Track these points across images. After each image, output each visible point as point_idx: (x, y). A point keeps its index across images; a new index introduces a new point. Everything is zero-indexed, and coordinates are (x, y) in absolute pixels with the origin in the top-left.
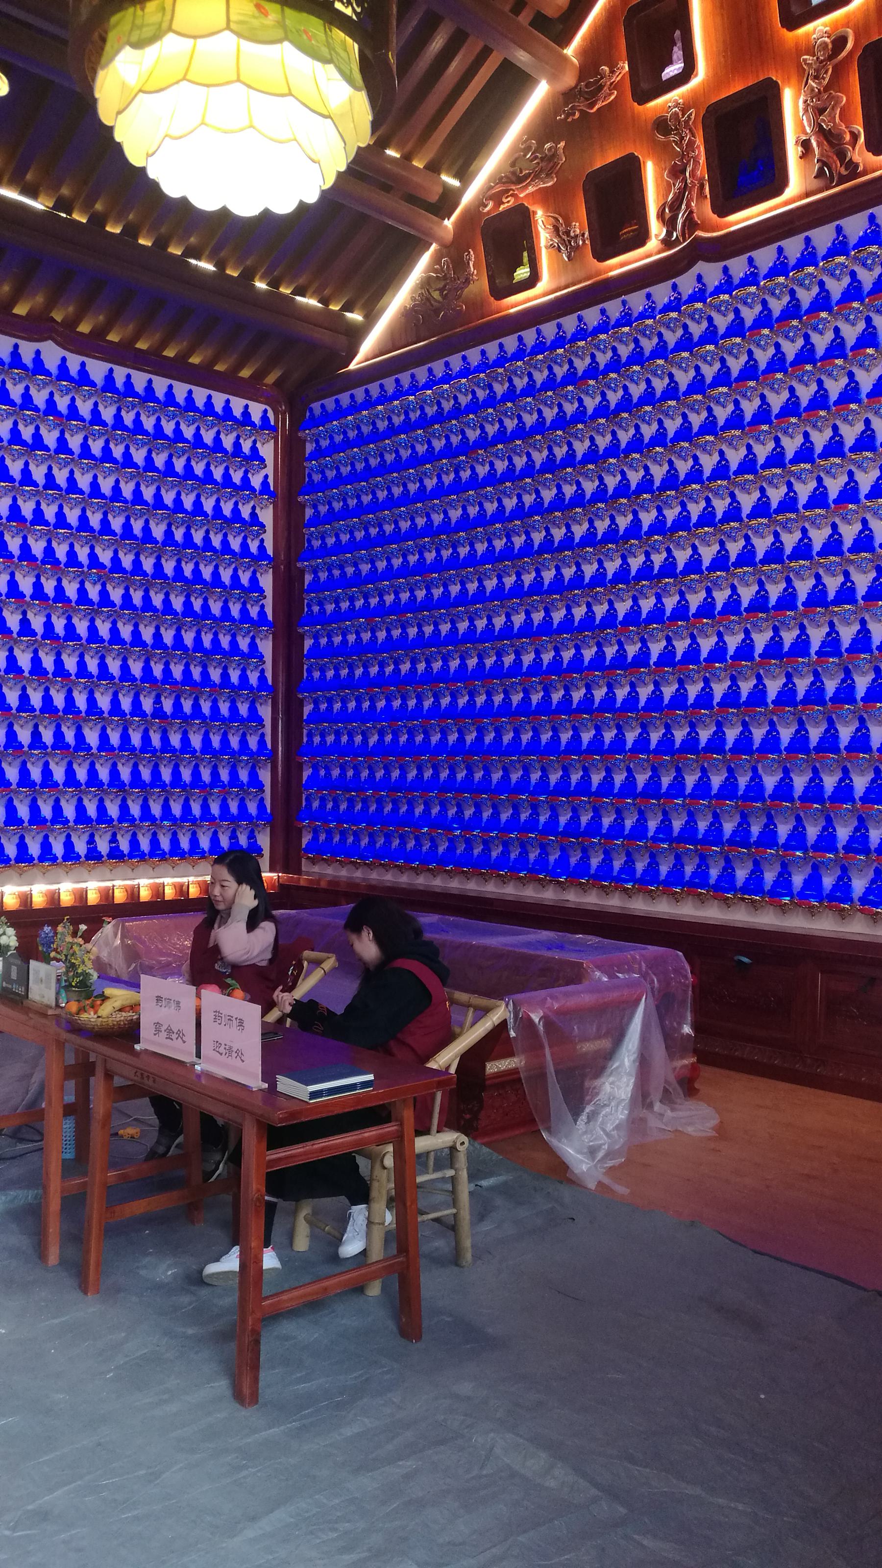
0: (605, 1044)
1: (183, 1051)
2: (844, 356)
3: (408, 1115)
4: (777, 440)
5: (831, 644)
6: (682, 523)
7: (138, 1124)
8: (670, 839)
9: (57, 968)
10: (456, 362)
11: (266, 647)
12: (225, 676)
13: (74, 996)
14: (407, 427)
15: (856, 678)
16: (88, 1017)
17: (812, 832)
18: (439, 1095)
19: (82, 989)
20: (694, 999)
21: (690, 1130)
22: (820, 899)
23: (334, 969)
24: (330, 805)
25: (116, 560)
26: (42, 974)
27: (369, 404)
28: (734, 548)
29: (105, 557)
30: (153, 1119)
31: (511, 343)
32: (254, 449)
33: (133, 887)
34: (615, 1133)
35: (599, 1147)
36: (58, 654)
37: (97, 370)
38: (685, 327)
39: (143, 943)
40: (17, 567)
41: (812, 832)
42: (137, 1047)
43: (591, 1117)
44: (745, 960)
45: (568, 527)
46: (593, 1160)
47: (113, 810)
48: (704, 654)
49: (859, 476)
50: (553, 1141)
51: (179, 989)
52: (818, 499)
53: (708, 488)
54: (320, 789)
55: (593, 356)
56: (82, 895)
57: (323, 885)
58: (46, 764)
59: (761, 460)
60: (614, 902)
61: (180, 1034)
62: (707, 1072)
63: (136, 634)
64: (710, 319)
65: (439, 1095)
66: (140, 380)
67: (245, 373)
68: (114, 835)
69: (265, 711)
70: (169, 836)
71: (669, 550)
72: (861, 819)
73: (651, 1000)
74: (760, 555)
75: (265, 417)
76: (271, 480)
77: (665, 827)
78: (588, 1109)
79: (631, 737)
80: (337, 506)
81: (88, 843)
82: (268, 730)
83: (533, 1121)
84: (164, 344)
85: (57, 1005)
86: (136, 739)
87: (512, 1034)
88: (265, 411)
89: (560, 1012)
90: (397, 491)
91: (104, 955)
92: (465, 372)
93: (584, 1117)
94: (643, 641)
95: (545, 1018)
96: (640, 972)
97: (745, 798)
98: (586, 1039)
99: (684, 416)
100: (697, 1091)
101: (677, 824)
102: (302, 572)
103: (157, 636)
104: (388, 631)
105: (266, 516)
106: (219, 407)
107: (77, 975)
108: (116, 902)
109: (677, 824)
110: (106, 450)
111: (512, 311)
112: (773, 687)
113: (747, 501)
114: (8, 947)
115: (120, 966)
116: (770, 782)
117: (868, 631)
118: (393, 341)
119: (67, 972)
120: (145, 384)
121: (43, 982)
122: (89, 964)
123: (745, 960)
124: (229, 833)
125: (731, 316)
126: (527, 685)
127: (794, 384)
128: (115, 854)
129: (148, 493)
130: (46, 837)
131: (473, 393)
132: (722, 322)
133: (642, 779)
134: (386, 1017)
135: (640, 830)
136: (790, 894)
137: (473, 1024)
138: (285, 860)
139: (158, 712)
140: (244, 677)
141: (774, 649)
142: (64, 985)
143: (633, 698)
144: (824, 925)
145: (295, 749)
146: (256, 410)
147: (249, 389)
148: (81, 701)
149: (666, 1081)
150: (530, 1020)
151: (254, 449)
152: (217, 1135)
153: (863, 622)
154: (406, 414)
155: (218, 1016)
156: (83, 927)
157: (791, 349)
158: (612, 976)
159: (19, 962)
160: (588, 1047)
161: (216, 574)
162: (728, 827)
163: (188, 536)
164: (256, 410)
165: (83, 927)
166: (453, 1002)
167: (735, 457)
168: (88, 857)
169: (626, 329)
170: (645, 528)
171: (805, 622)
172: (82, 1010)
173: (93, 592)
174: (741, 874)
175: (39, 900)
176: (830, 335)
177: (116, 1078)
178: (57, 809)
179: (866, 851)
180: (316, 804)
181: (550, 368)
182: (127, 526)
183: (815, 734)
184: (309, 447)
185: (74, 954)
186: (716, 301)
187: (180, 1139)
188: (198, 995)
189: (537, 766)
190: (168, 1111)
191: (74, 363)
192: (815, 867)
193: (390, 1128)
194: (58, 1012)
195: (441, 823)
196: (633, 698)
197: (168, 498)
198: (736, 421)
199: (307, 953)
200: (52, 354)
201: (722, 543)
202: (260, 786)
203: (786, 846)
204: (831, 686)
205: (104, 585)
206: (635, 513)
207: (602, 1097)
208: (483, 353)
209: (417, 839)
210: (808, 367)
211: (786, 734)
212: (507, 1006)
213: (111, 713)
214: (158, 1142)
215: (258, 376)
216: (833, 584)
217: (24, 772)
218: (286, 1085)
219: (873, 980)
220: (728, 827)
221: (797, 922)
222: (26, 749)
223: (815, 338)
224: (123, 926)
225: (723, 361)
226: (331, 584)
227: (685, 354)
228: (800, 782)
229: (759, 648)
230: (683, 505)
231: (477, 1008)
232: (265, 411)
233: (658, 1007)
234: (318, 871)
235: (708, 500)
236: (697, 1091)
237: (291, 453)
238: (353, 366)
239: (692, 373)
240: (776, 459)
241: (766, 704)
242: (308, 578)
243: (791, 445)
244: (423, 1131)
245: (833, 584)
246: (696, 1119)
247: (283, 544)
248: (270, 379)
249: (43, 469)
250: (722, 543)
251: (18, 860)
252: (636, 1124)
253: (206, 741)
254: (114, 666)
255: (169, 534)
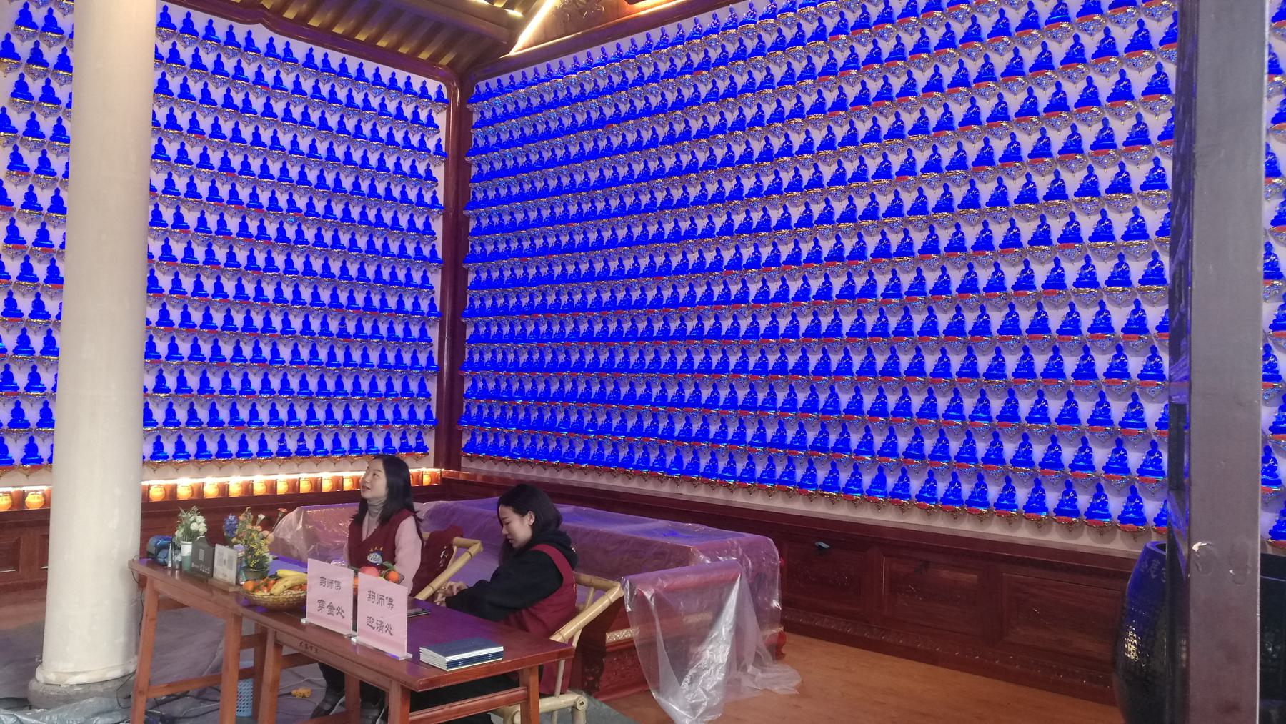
0: (708, 616)
1: (341, 625)
2: (904, 59)
3: (534, 680)
4: (852, 123)
5: (894, 287)
6: (776, 188)
7: (307, 687)
8: (764, 445)
9: (240, 549)
10: (596, 52)
11: (436, 280)
12: (400, 303)
13: (251, 576)
14: (556, 104)
15: (914, 316)
16: (263, 594)
17: (879, 440)
18: (562, 663)
19: (258, 570)
20: (782, 578)
21: (776, 689)
22: (885, 494)
23: (479, 553)
24: (486, 412)
25: (310, 205)
26: (226, 557)
27: (525, 84)
28: (817, 209)
29: (301, 203)
30: (323, 682)
31: (640, 39)
32: (430, 118)
33: (316, 480)
34: (713, 692)
35: (699, 705)
36: (259, 282)
37: (300, 49)
38: (780, 31)
39: (322, 528)
40: (226, 209)
41: (879, 440)
42: (303, 621)
43: (694, 679)
44: (824, 545)
45: (685, 188)
46: (695, 714)
47: (302, 414)
48: (792, 294)
49: (916, 154)
50: (662, 700)
51: (340, 571)
52: (884, 172)
53: (797, 160)
54: (479, 398)
55: (706, 52)
56: (272, 486)
57: (479, 479)
58: (246, 375)
59: (839, 139)
60: (719, 496)
61: (340, 611)
62: (792, 638)
63: (326, 267)
64: (799, 26)
65: (562, 663)
66: (335, 58)
67: (424, 56)
68: (302, 435)
69: (433, 333)
70: (349, 436)
71: (765, 210)
72: (917, 431)
73: (745, 581)
74: (837, 215)
75: (439, 93)
76: (443, 143)
77: (761, 435)
78: (692, 672)
79: (734, 360)
80: (498, 166)
81: (280, 441)
82: (435, 349)
83: (645, 682)
84: (356, 30)
85: (238, 583)
86: (323, 355)
87: (628, 609)
88: (440, 87)
89: (667, 590)
90: (547, 155)
91: (288, 537)
92: (605, 61)
93: (687, 679)
94: (744, 282)
95: (655, 595)
96: (737, 555)
97: (824, 411)
98: (688, 613)
99: (778, 102)
100: (783, 655)
101: (770, 433)
102: (468, 219)
103: (344, 269)
104: (538, 268)
105: (439, 172)
106: (401, 83)
107: (256, 558)
108: (302, 491)
109: (770, 433)
110: (305, 115)
111: (642, 13)
112: (847, 322)
113: (828, 172)
114: (197, 533)
115: (300, 546)
116: (845, 399)
117: (923, 278)
118: (545, 34)
119: (246, 555)
120: (340, 62)
121: (226, 563)
122: (266, 549)
123: (824, 545)
124: (400, 435)
125: (816, 24)
126: (651, 315)
127: (866, 79)
128: (302, 451)
129: (340, 152)
130: (243, 436)
131: (610, 78)
132: (809, 29)
133: (742, 394)
134: (516, 595)
135: (740, 437)
136: (861, 491)
137: (594, 600)
138: (447, 457)
139: (342, 333)
140: (416, 304)
141: (848, 292)
142: (243, 567)
143: (735, 328)
144: (888, 517)
145: (459, 364)
146: (432, 86)
147: (427, 69)
148: (277, 323)
149: (758, 648)
150: (644, 597)
151: (430, 118)
152: (373, 696)
153: (919, 271)
154: (555, 93)
155: (371, 595)
156: (262, 517)
157: (863, 52)
158: (714, 559)
159: (206, 546)
160: (693, 619)
161: (395, 219)
162: (811, 436)
163: (372, 187)
164: (432, 86)
165: (262, 517)
166: (578, 582)
167: (818, 137)
168: (279, 454)
169: (733, 31)
170: (746, 191)
171: (873, 270)
172: (257, 588)
173: (291, 232)
174: (822, 474)
175: (259, 489)
176: (893, 42)
177: (285, 648)
178: (254, 413)
179: (922, 457)
180: (474, 411)
181: (672, 60)
182: (321, 178)
183: (881, 360)
184: (476, 118)
185: (253, 540)
186: (804, 12)
187: (342, 699)
188: (356, 576)
189: (658, 382)
190: (335, 679)
191: (280, 42)
192: (881, 469)
193: (518, 692)
194: (237, 589)
195: (578, 428)
196: (735, 328)
197: (357, 156)
198: (819, 108)
199: (457, 540)
200: (261, 35)
201: (807, 205)
202: (428, 395)
203: (858, 452)
204: (893, 322)
205: (300, 226)
206: (738, 179)
207: (703, 662)
208: (618, 46)
209: (558, 441)
210: (877, 66)
211: (857, 360)
212: (623, 587)
213: (303, 333)
214: (325, 701)
215: (434, 59)
216: (895, 240)
217: (226, 381)
218: (427, 655)
219: (927, 564)
220: (811, 436)
221: (866, 515)
222: (228, 361)
223: (881, 43)
224: (305, 515)
225: (809, 59)
226: (491, 229)
227: (780, 53)
228: (868, 400)
229: (836, 290)
230: (777, 173)
231: (597, 588)
232: (440, 87)
233: (751, 586)
234: (474, 468)
235: (796, 170)
236: (783, 655)
237: (461, 122)
238: (513, 53)
239: (785, 68)
240: (851, 139)
241: (841, 335)
242: (473, 224)
243: (863, 128)
244: (548, 692)
245: (895, 240)
246: (781, 680)
247: (452, 195)
248: (445, 61)
249: (251, 129)
250: (807, 205)
251: (219, 455)
252: (731, 684)
253: (383, 357)
254: (306, 294)
255: (356, 185)
